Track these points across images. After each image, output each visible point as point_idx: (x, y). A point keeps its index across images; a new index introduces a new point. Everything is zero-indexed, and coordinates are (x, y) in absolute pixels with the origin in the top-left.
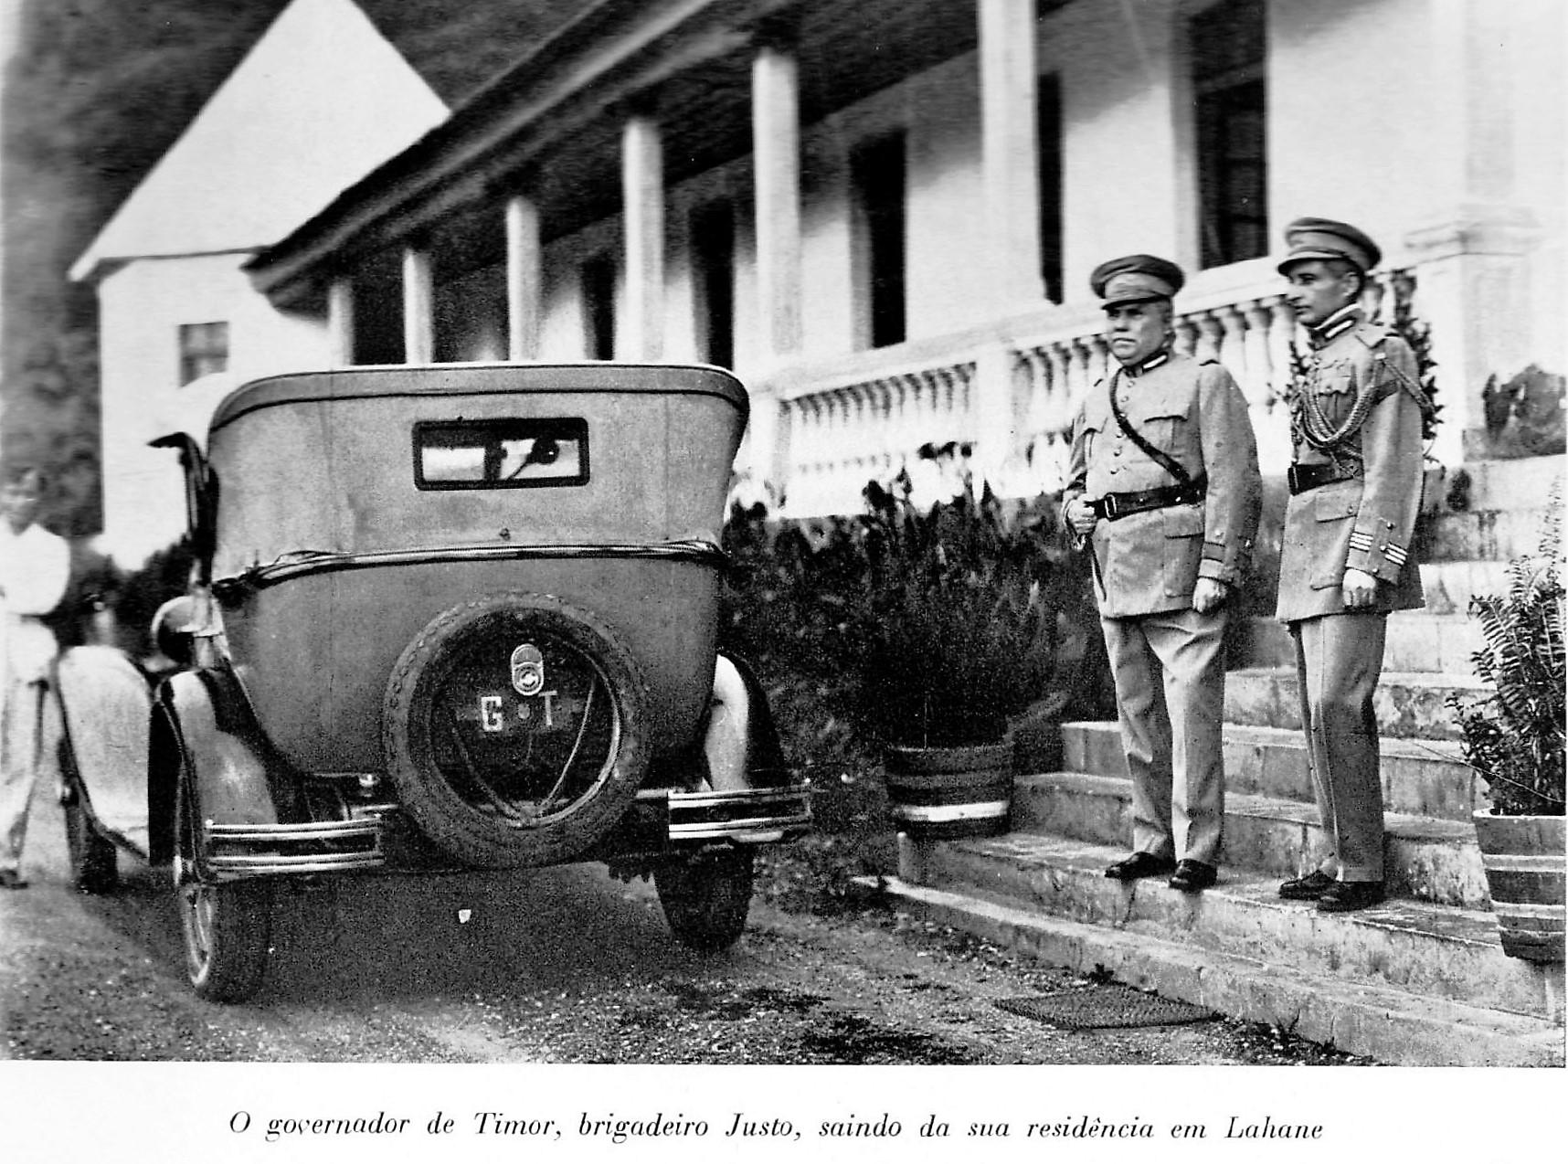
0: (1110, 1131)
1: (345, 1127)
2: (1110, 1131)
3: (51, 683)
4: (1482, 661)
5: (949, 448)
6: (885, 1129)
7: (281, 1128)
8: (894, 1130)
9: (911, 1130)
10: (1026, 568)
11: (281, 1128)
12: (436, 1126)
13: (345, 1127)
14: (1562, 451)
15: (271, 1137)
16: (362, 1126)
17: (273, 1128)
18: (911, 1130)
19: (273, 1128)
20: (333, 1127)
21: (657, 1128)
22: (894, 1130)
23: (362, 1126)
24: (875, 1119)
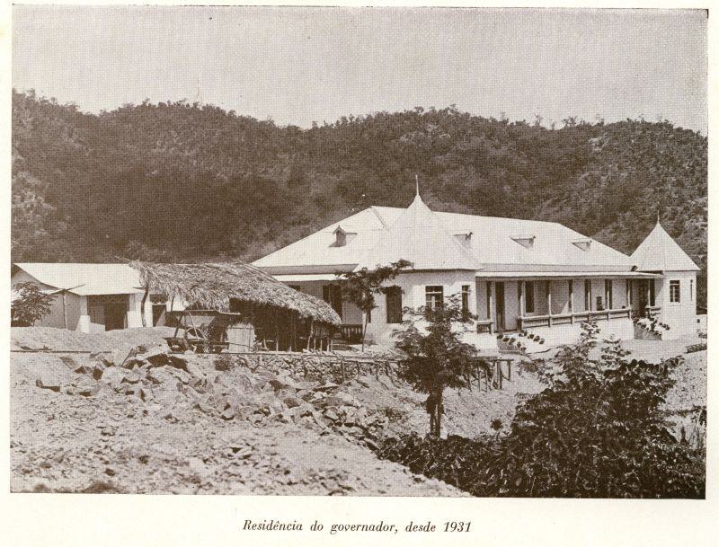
0: (283, 527)
1: (365, 528)
2: (283, 527)
3: (162, 319)
4: (188, 105)
5: (536, 340)
6: (429, 528)
7: (337, 529)
8: (320, 527)
9: (306, 527)
10: (486, 345)
11: (337, 529)
12: (315, 527)
13: (365, 528)
14: (693, 489)
15: (333, 532)
16: (373, 528)
17: (334, 528)
18: (306, 527)
19: (334, 528)
20: (360, 528)
21: (271, 527)
22: (320, 527)
23: (373, 528)
24: (377, 523)
